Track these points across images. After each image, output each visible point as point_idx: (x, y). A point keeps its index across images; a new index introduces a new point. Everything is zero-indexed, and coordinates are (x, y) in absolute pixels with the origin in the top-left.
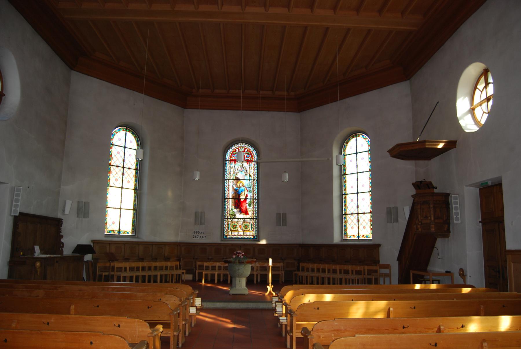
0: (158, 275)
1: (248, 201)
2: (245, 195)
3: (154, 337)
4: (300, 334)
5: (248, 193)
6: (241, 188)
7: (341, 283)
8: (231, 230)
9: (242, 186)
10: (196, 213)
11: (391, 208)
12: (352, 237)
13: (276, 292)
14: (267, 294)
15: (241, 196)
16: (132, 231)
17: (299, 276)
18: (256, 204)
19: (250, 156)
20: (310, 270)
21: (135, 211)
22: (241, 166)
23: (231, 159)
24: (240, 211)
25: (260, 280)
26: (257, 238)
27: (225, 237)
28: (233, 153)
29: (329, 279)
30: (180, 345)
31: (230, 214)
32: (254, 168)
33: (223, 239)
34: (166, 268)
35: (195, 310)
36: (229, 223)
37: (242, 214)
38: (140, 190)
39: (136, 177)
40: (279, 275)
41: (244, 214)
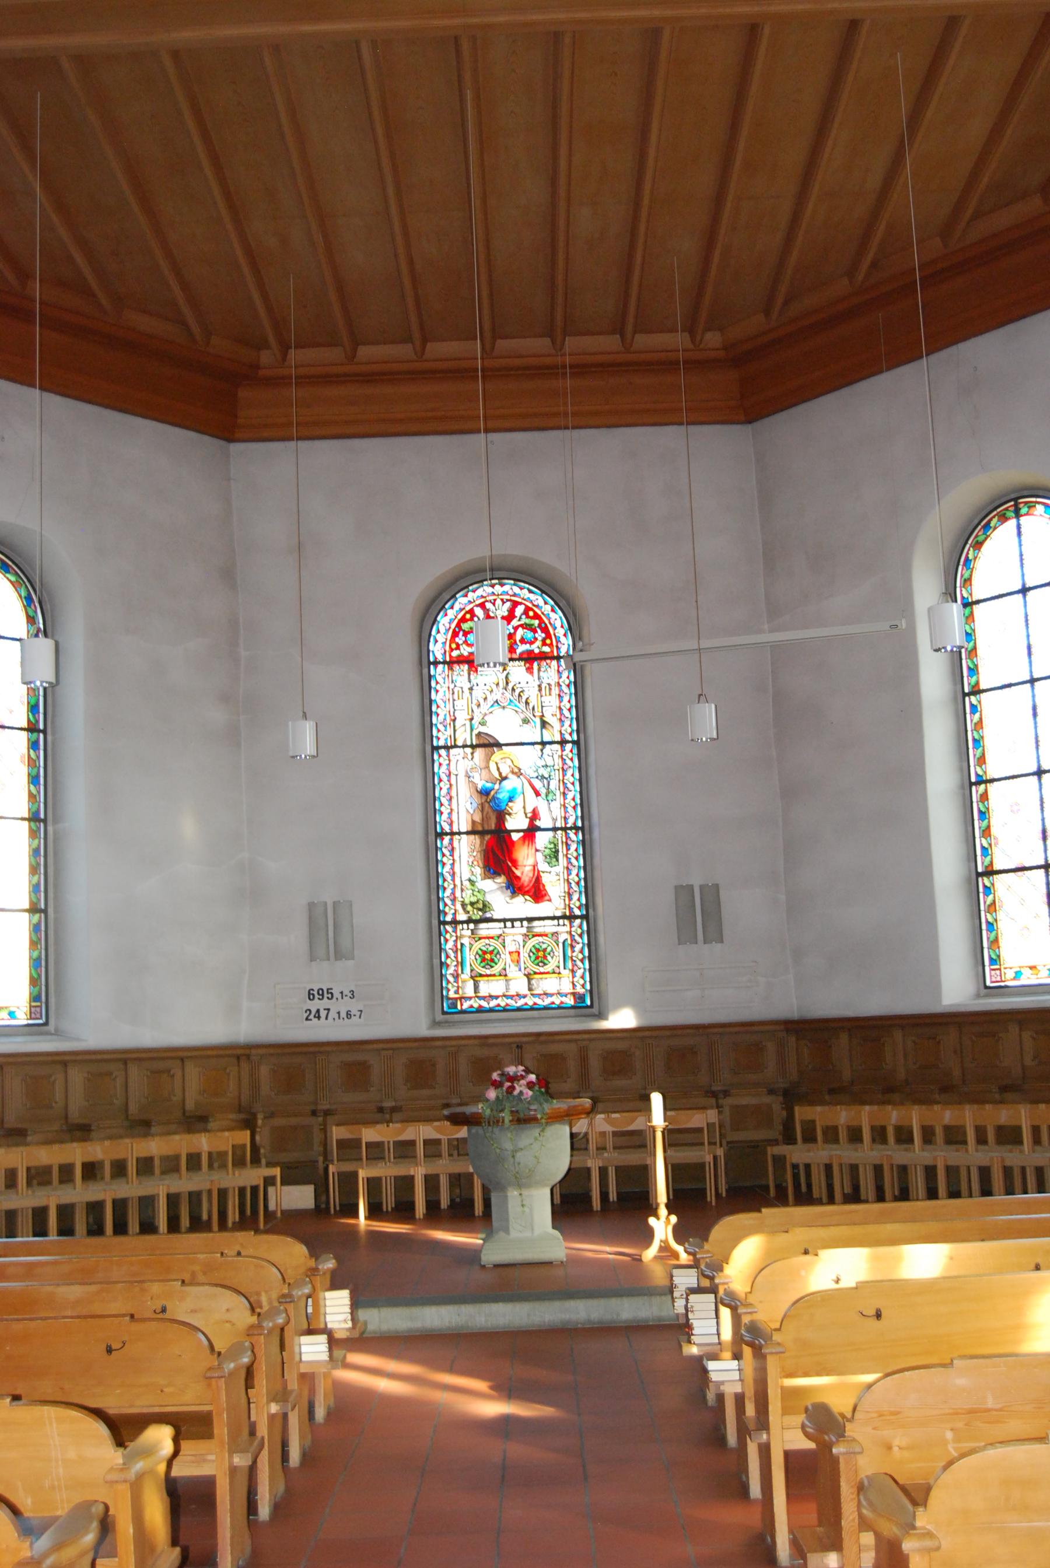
0: (158, 1195)
1: (542, 839)
2: (526, 814)
3: (136, 1487)
4: (799, 1434)
5: (541, 804)
6: (504, 783)
7: (986, 1192)
8: (475, 977)
9: (513, 772)
10: (311, 906)
12: (1027, 972)
13: (687, 1245)
14: (650, 1253)
15: (507, 817)
16: (31, 1007)
17: (795, 1167)
18: (581, 851)
19: (540, 635)
20: (843, 1135)
21: (37, 916)
22: (501, 685)
23: (455, 653)
24: (508, 888)
25: (618, 1194)
26: (592, 1006)
27: (449, 1008)
28: (460, 629)
29: (930, 1172)
30: (264, 1512)
31: (467, 901)
32: (561, 690)
33: (440, 1017)
34: (194, 1161)
35: (324, 1347)
36: (462, 945)
37: (520, 898)
38: (55, 821)
39: (32, 763)
40: (702, 1166)
41: (527, 897)
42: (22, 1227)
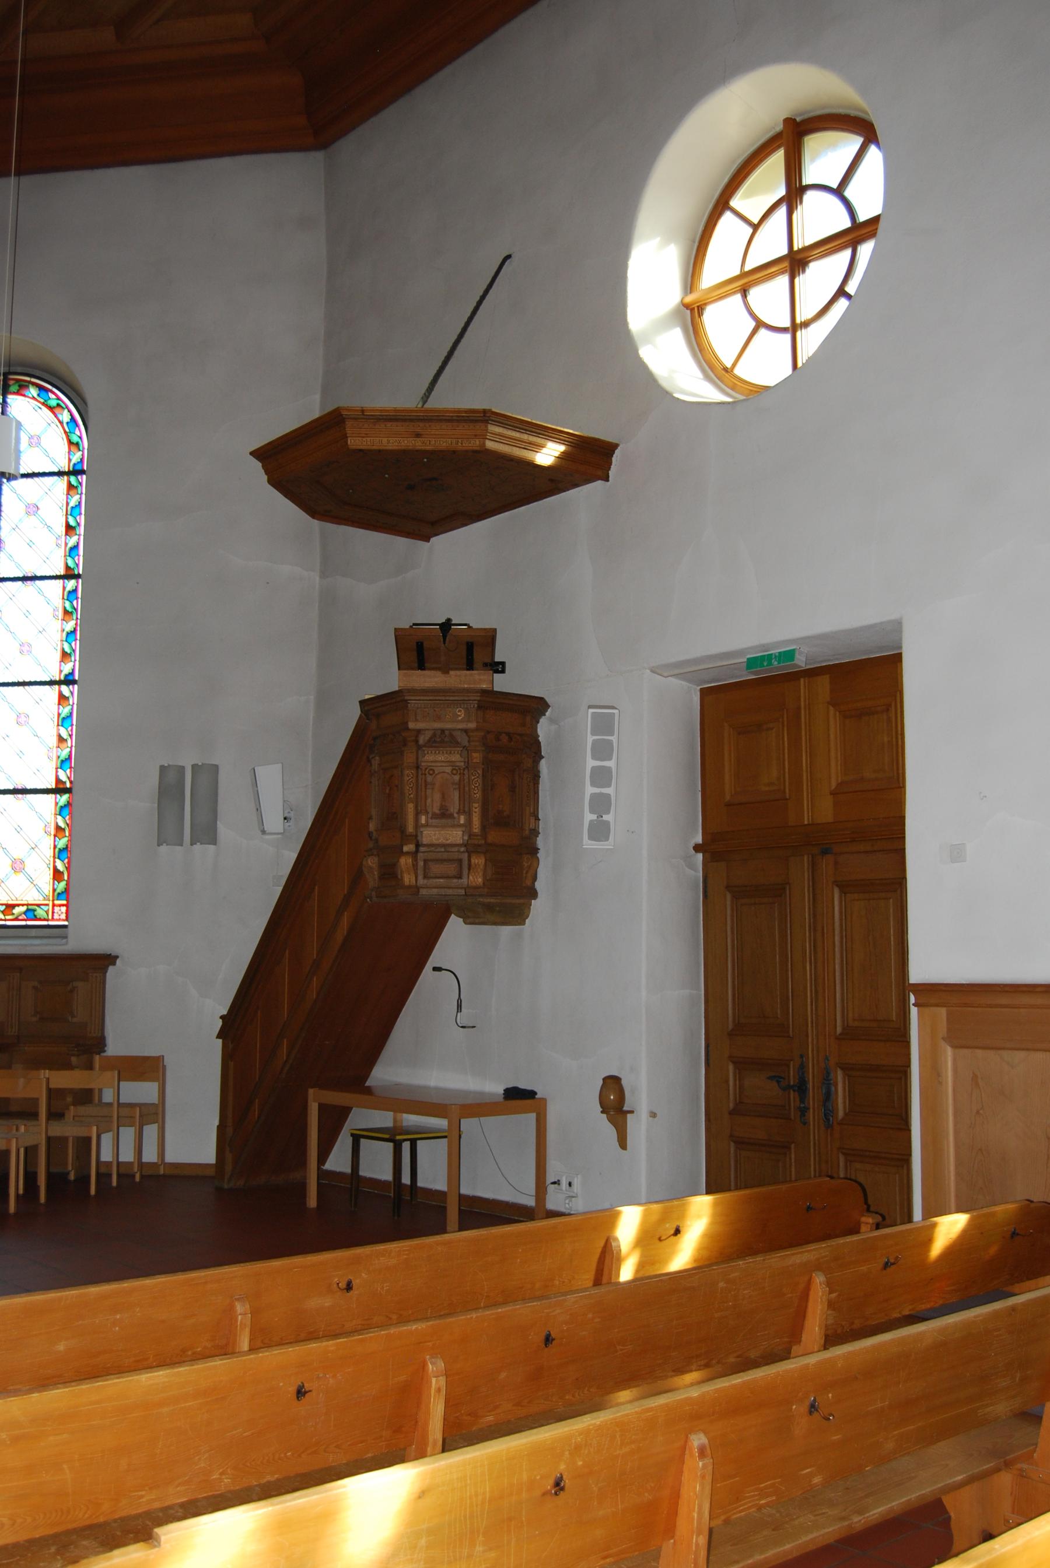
11: (182, 769)
42: (430, 700)
